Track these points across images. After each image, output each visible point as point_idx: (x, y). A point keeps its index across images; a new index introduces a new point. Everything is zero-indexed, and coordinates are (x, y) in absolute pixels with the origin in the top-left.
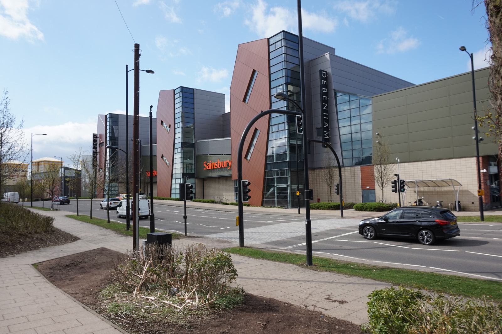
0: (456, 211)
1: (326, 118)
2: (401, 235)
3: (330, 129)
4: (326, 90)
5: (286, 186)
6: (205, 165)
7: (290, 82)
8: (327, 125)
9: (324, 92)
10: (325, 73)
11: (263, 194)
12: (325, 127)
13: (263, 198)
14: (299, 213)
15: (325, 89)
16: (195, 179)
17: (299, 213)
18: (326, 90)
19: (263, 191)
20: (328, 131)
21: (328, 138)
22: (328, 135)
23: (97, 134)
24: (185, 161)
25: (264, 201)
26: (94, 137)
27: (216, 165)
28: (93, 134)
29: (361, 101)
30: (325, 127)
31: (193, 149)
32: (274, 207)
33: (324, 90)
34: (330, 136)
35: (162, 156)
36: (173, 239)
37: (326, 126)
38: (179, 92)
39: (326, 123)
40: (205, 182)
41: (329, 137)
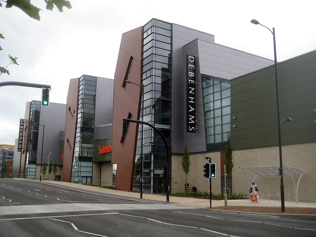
0: (295, 201)
1: (192, 102)
2: (219, 233)
3: (196, 114)
4: (193, 75)
5: (148, 171)
6: (99, 149)
7: (167, 68)
8: (192, 109)
9: (191, 76)
10: (193, 58)
11: (132, 178)
12: (190, 111)
13: (132, 182)
14: (141, 197)
15: (192, 73)
16: (93, 163)
17: (141, 197)
18: (193, 75)
19: (133, 174)
20: (194, 115)
21: (194, 122)
22: (194, 119)
23: (24, 120)
24: (84, 145)
25: (134, 185)
26: (21, 122)
27: (107, 149)
28: (21, 119)
29: (223, 84)
30: (190, 111)
31: (93, 133)
32: (150, 193)
33: (191, 74)
34: (196, 121)
35: (68, 141)
36: (280, 207)
37: (191, 110)
38: (150, 106)
39: (191, 108)
40: (102, 166)
41: (195, 121)
